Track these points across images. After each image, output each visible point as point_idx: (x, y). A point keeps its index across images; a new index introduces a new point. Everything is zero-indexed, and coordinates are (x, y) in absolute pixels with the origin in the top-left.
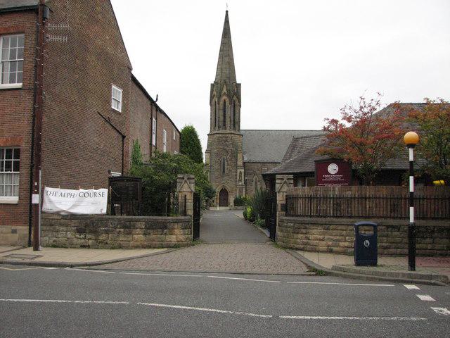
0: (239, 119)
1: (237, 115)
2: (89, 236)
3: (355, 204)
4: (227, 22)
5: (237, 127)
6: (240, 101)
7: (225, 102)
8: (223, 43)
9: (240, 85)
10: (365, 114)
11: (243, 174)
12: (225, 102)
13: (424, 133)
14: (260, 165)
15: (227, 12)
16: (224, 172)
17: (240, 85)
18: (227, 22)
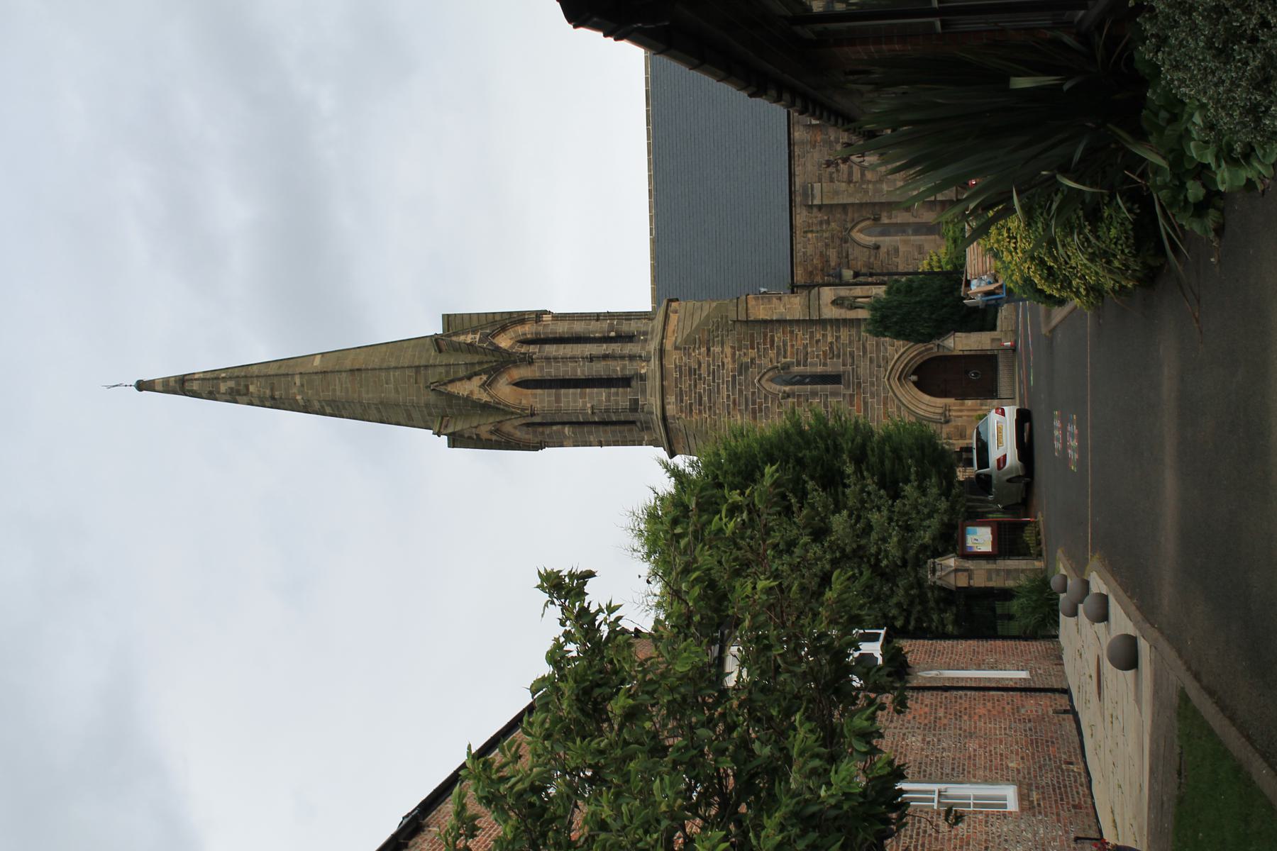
0: (598, 317)
1: (579, 327)
2: (962, 582)
3: (1014, 245)
4: (181, 386)
5: (633, 327)
6: (518, 318)
7: (523, 384)
8: (212, 396)
9: (448, 319)
10: (968, 283)
11: (843, 292)
12: (523, 384)
13: (1032, 664)
14: (801, 217)
15: (142, 386)
16: (834, 379)
17: (448, 319)
18: (181, 386)
